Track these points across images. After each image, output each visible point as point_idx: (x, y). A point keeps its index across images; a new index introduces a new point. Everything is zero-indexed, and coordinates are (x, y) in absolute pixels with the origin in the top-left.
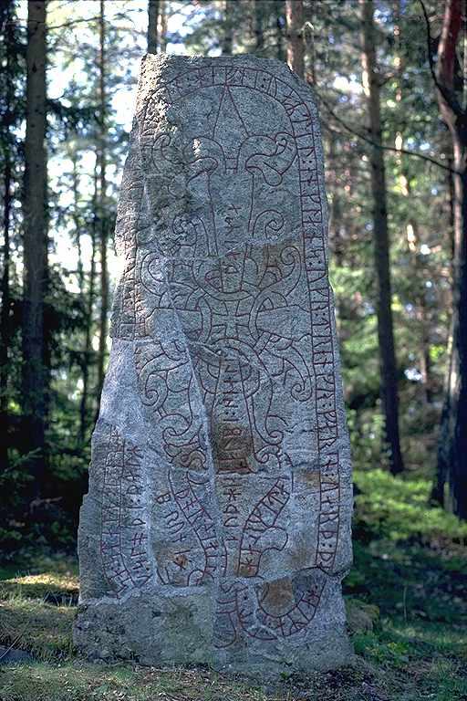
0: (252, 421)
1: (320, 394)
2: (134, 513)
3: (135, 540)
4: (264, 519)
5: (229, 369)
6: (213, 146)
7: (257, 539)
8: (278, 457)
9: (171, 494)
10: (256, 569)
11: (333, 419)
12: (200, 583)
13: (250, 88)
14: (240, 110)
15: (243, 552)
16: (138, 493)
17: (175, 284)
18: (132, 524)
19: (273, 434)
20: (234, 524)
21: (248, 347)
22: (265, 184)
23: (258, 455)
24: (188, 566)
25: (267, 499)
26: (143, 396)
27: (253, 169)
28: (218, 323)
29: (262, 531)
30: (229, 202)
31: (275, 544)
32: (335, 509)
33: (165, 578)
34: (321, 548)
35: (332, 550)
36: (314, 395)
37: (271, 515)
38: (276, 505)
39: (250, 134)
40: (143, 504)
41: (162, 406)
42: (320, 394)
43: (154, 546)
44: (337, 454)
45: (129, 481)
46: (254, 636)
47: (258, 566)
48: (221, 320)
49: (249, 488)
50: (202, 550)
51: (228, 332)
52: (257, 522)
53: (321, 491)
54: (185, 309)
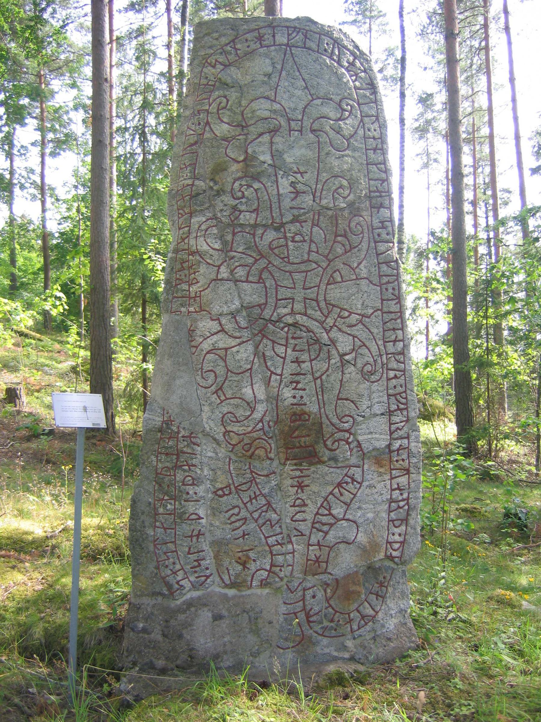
0: (322, 405)
1: (392, 374)
2: (191, 507)
3: (191, 536)
4: (334, 512)
5: (297, 348)
6: (276, 106)
7: (326, 533)
8: (349, 444)
9: (232, 487)
10: (324, 565)
11: (404, 401)
12: (264, 584)
13: (314, 51)
14: (302, 71)
15: (311, 548)
16: (193, 484)
17: (235, 254)
18: (188, 519)
19: (344, 420)
20: (301, 518)
21: (317, 324)
22: (330, 148)
23: (329, 443)
24: (253, 567)
25: (337, 490)
26: (199, 378)
27: (319, 133)
28: (284, 297)
29: (331, 525)
30: (294, 165)
31: (344, 537)
32: (405, 496)
33: (226, 578)
34: (391, 538)
35: (401, 539)
36: (385, 375)
37: (342, 507)
38: (347, 497)
39: (314, 97)
40: (201, 497)
41: (221, 388)
42: (392, 374)
43: (213, 543)
44: (408, 438)
45: (185, 471)
46: (322, 635)
47: (327, 562)
48: (288, 293)
49: (318, 479)
50: (267, 548)
51: (295, 306)
52: (326, 515)
53: (392, 478)
54: (247, 281)
